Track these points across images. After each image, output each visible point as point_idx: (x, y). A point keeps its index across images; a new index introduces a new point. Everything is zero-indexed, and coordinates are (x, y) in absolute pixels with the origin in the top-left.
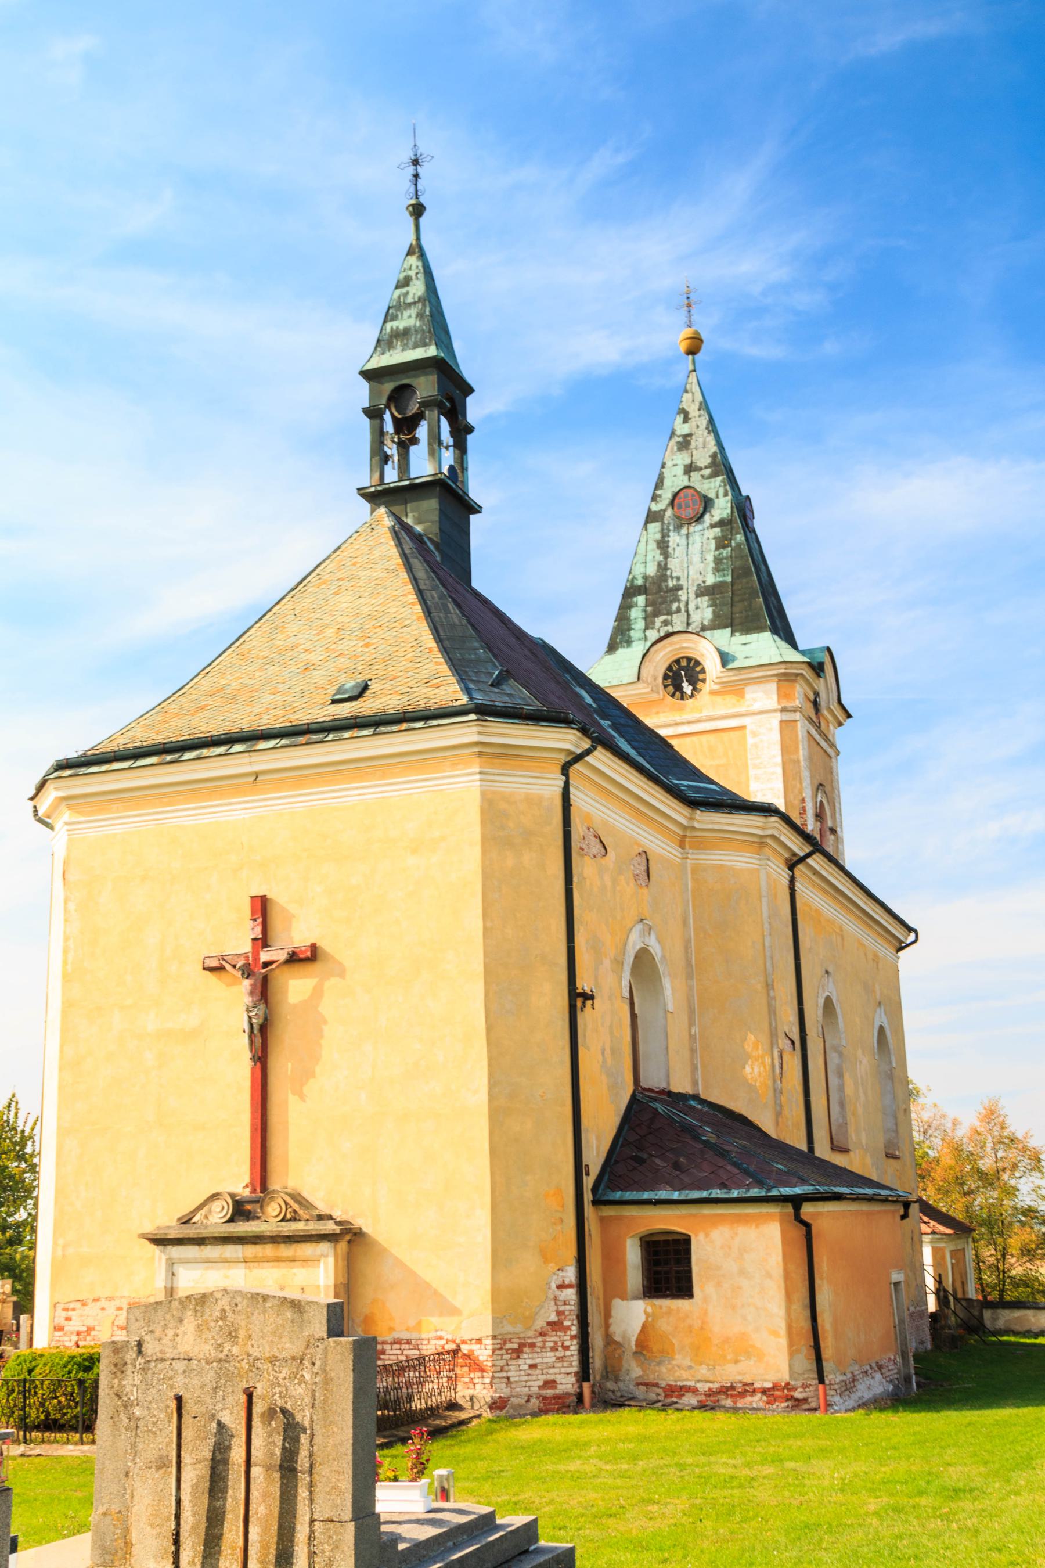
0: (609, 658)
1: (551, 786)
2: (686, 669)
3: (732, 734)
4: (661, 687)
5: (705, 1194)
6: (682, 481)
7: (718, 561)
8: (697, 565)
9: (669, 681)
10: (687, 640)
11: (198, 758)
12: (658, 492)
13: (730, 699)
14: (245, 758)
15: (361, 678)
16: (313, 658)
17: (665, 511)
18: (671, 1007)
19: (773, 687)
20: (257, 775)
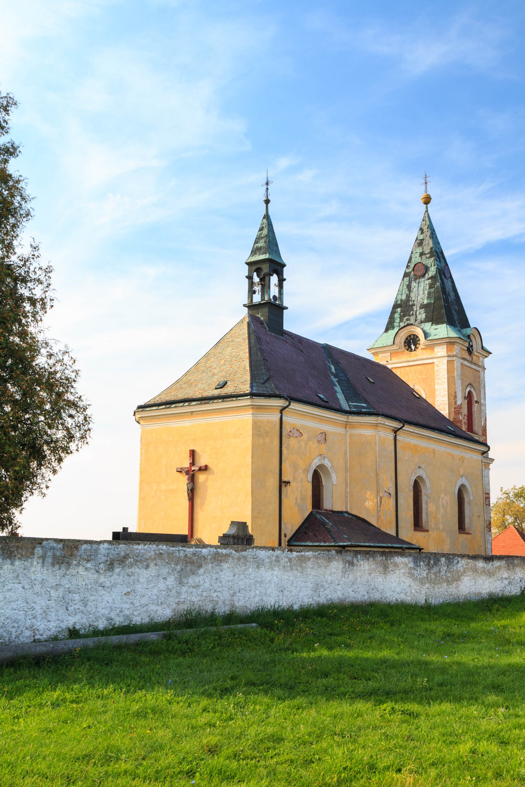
0: (385, 334)
1: (276, 417)
2: (413, 339)
3: (429, 365)
4: (403, 347)
5: (318, 544)
6: (418, 260)
7: (429, 294)
8: (421, 296)
9: (406, 344)
10: (413, 328)
11: (175, 407)
12: (409, 264)
13: (429, 351)
14: (188, 407)
15: (226, 380)
16: (215, 371)
17: (411, 272)
18: (335, 483)
19: (445, 347)
20: (192, 412)
